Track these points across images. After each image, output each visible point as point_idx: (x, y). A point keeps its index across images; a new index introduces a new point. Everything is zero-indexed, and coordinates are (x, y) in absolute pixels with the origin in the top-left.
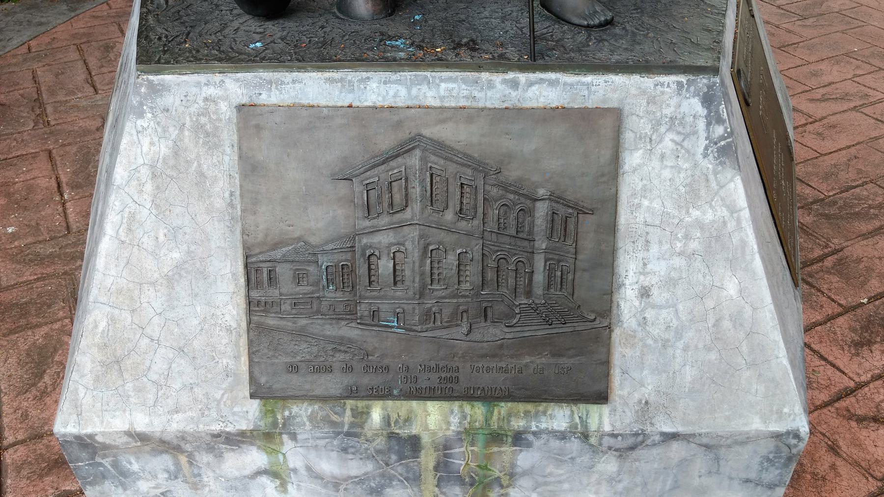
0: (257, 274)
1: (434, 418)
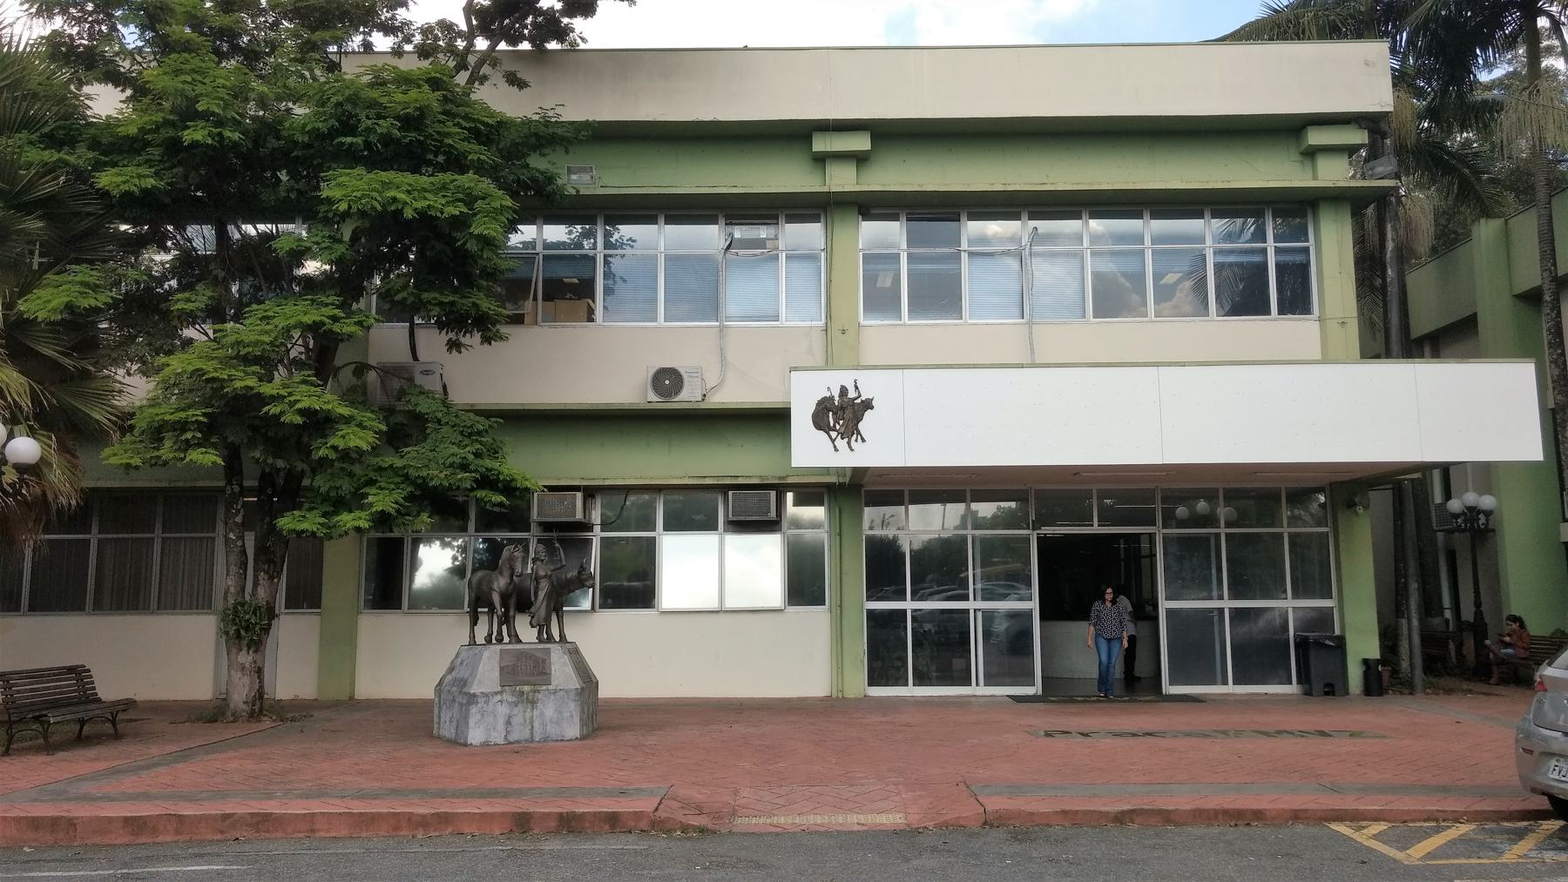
0: (502, 669)
1: (526, 688)
